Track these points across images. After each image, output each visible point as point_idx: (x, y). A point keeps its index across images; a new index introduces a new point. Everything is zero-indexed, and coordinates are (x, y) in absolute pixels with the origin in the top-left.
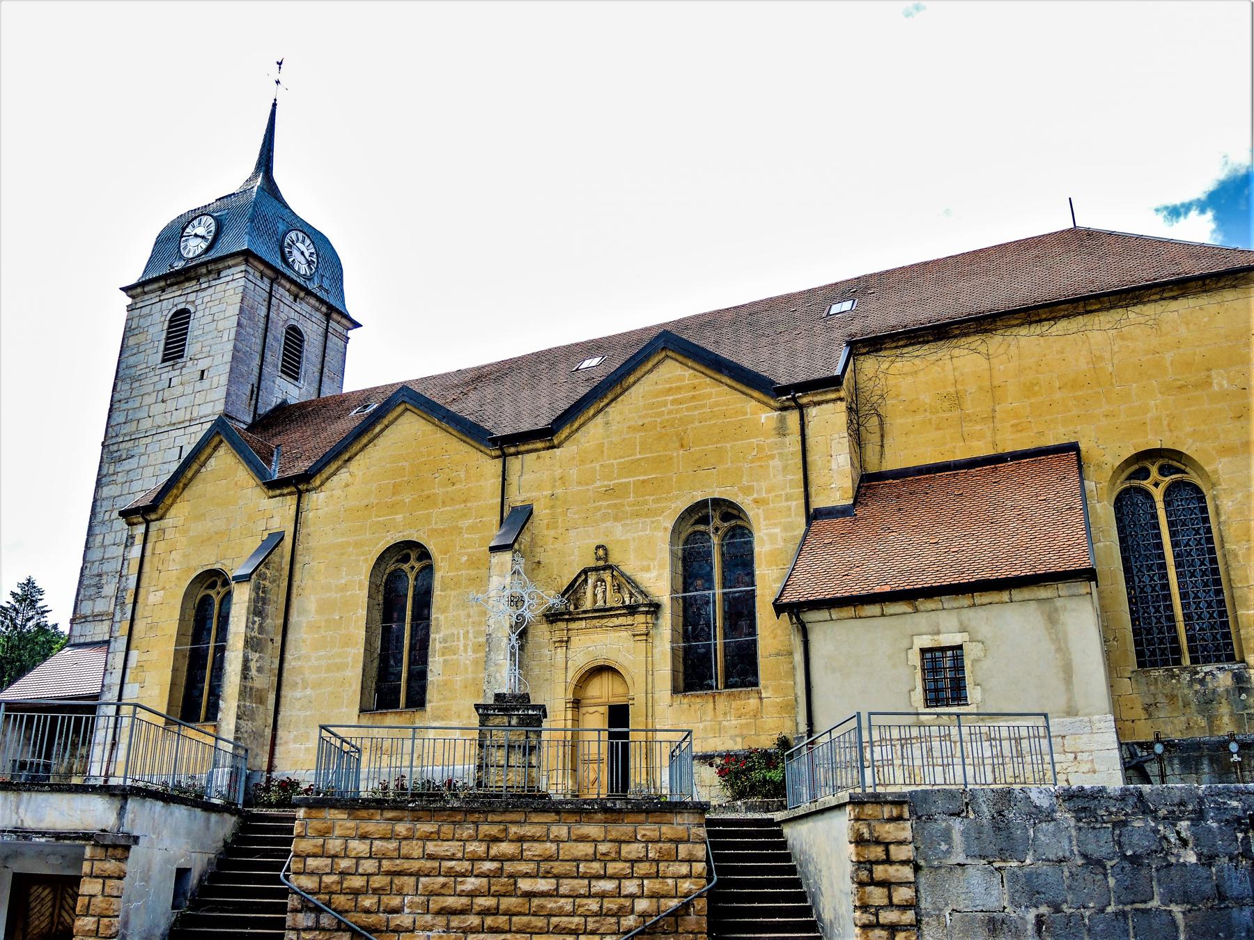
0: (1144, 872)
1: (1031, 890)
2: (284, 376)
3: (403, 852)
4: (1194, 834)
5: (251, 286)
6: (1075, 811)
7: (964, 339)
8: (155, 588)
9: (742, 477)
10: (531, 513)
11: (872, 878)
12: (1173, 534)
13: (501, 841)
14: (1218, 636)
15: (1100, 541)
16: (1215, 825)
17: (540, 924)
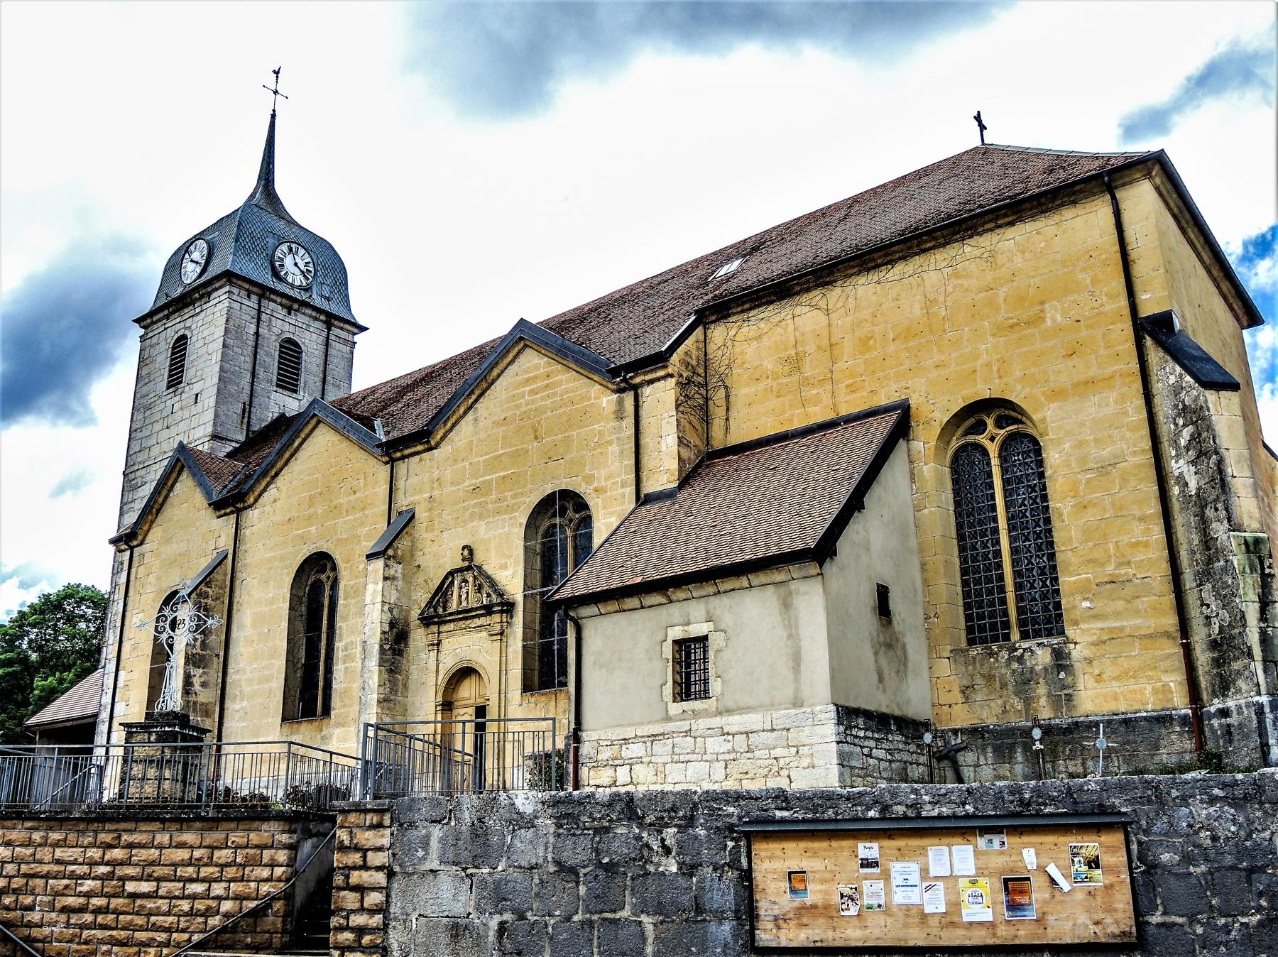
0: (618, 880)
1: (498, 897)
2: (280, 390)
3: (38, 857)
4: (678, 842)
5: (236, 306)
6: (556, 818)
7: (805, 296)
8: (136, 611)
9: (585, 466)
10: (413, 517)
11: (348, 883)
12: (1007, 493)
13: (115, 847)
14: (1051, 607)
15: (925, 507)
16: (703, 832)
17: (140, 922)
